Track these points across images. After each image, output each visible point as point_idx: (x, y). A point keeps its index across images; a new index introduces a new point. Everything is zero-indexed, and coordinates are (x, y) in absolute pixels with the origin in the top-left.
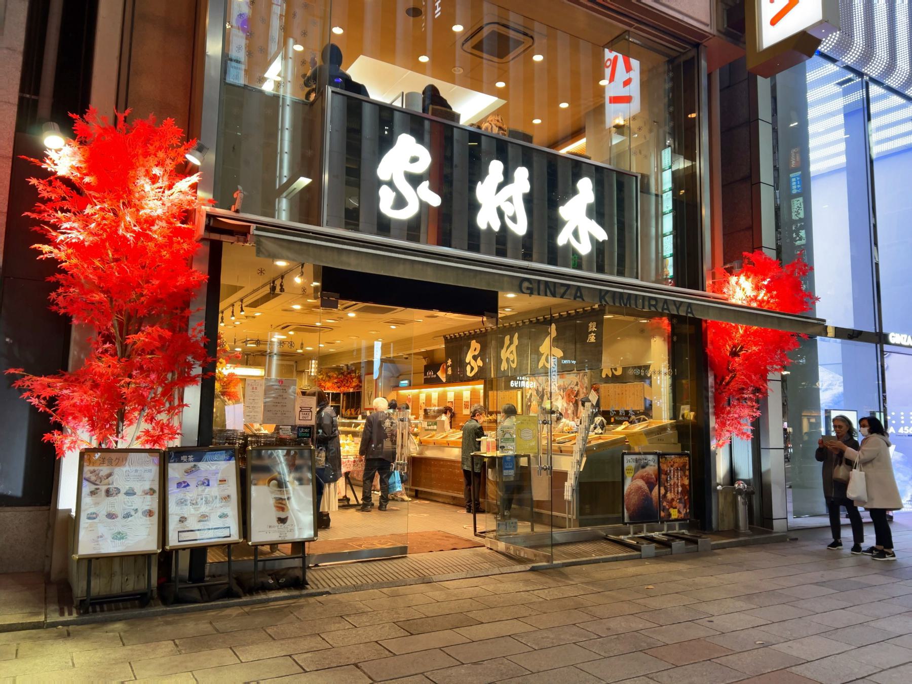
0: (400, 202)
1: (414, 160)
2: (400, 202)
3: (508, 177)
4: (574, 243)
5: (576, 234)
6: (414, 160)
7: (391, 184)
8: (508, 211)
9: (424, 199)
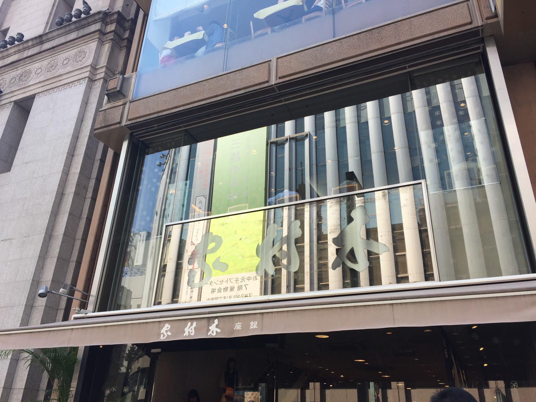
0: (164, 336)
1: (168, 328)
2: (164, 336)
3: (192, 325)
4: (212, 334)
5: (213, 332)
6: (168, 328)
7: (163, 333)
8: (191, 332)
9: (168, 334)
